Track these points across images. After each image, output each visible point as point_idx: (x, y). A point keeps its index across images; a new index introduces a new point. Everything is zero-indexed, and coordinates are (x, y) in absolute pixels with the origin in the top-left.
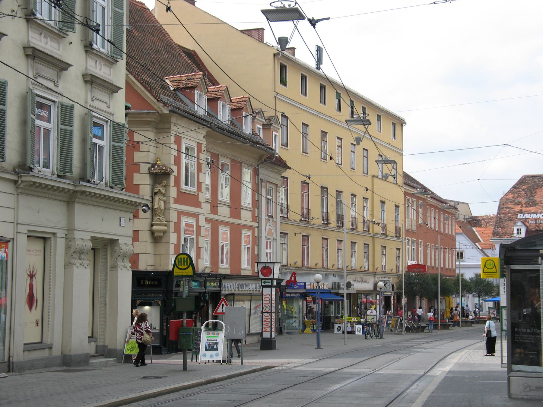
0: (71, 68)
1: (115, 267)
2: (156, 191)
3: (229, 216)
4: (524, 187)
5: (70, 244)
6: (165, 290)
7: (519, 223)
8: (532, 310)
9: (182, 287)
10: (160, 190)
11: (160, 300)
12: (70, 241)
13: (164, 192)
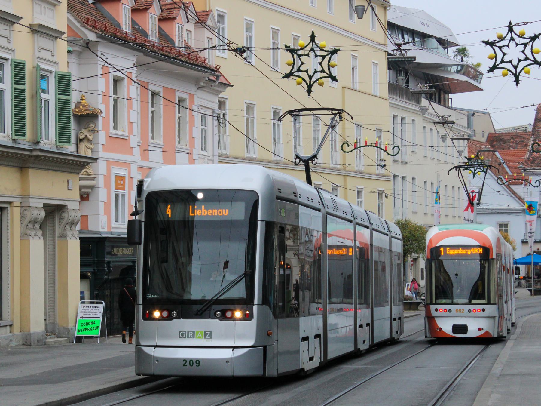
1: (63, 236)
2: (81, 137)
3: (162, 162)
5: (25, 213)
6: (96, 259)
9: (532, 276)
10: (86, 136)
11: (90, 272)
12: (25, 210)
13: (91, 138)
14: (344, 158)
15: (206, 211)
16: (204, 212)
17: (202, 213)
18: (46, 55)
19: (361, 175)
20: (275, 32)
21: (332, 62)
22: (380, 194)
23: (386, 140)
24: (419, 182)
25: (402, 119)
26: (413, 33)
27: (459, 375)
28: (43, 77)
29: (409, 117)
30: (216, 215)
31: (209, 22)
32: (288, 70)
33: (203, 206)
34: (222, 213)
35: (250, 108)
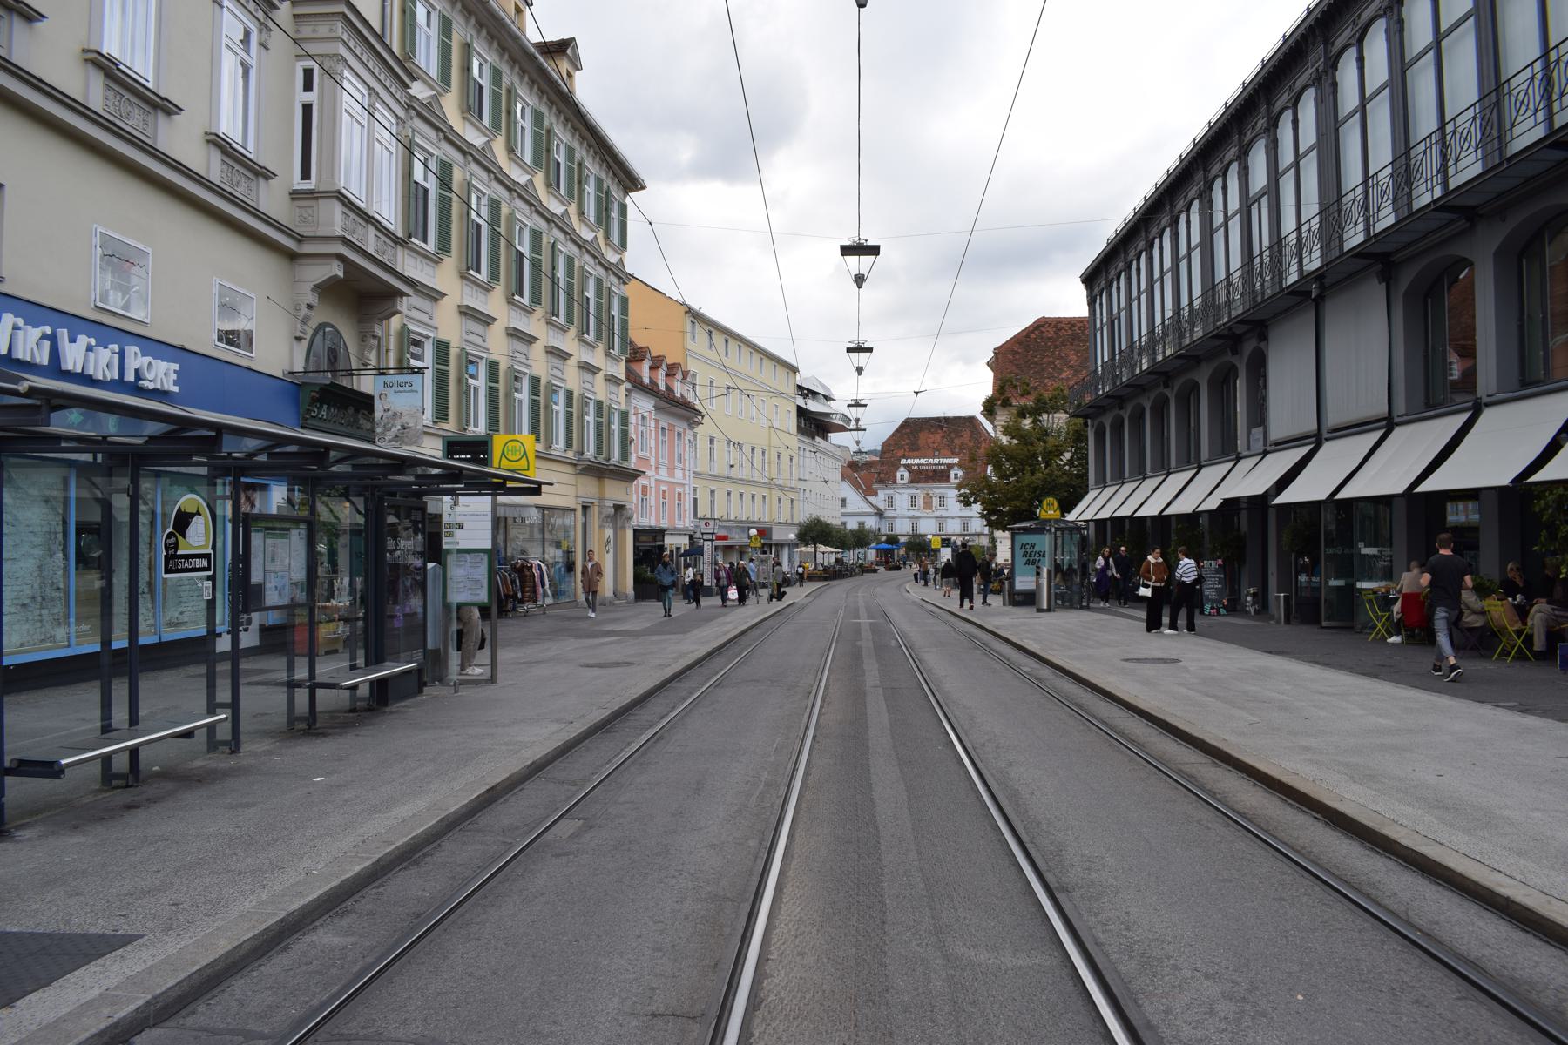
0: (496, 323)
4: (908, 431)
7: (902, 469)
8: (1522, 594)
18: (558, 373)
28: (471, 362)
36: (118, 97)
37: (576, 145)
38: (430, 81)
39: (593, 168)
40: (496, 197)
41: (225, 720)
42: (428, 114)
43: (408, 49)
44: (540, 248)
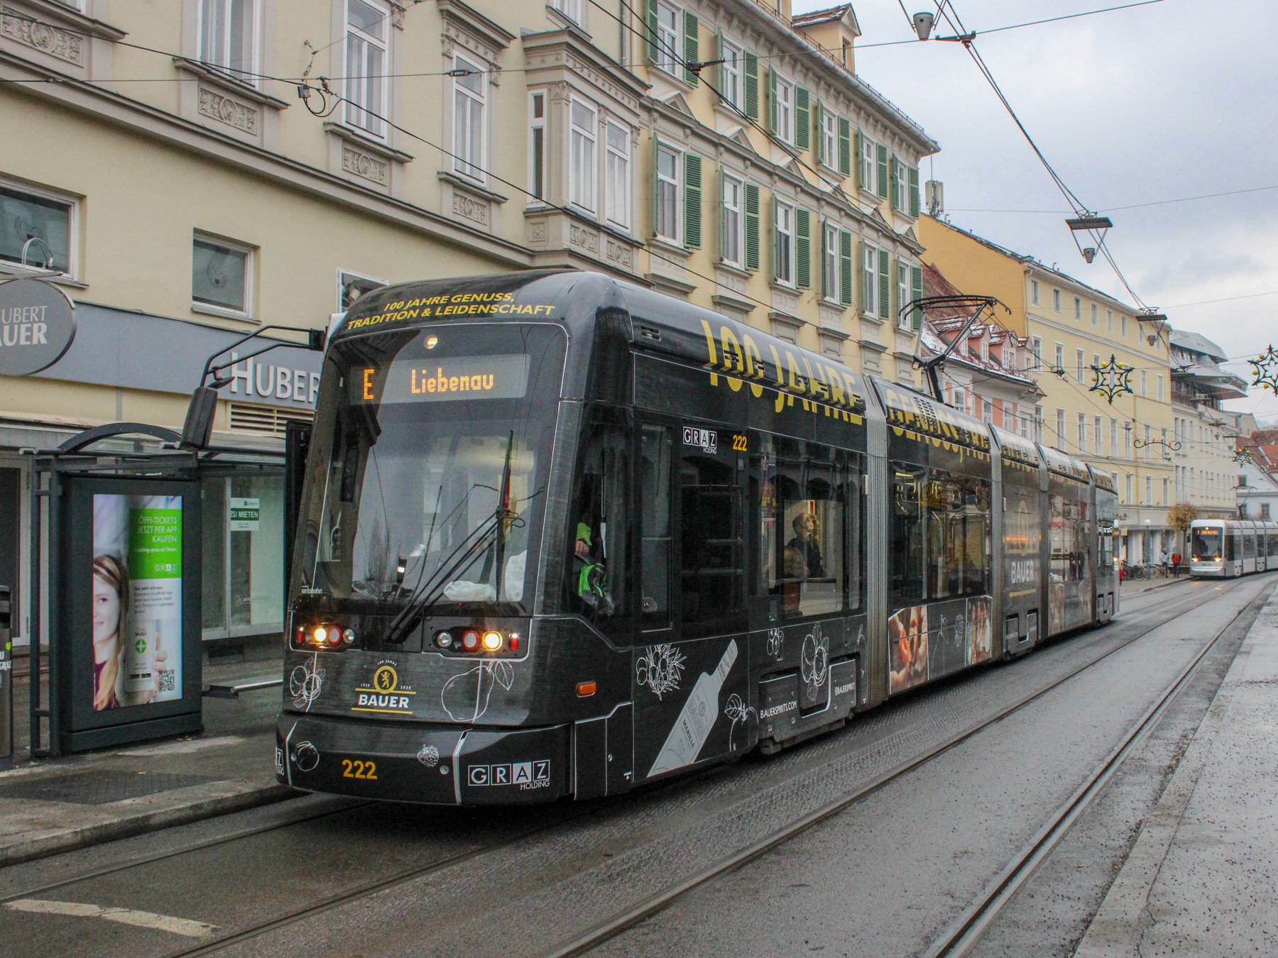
14: (1136, 452)
15: (445, 380)
16: (443, 384)
17: (436, 387)
18: (873, 366)
19: (1150, 466)
20: (1080, 354)
21: (1129, 378)
22: (1165, 480)
23: (1169, 437)
24: (1196, 471)
25: (1183, 421)
26: (1190, 352)
27: (1146, 722)
29: (1188, 419)
30: (467, 389)
31: (1028, 346)
32: (1093, 385)
33: (440, 370)
34: (479, 384)
35: (1060, 413)
36: (356, 156)
37: (887, 143)
38: (662, 74)
39: (873, 137)
40: (848, 231)
41: (851, 692)
42: (674, 115)
43: (649, 54)
44: (699, 178)
